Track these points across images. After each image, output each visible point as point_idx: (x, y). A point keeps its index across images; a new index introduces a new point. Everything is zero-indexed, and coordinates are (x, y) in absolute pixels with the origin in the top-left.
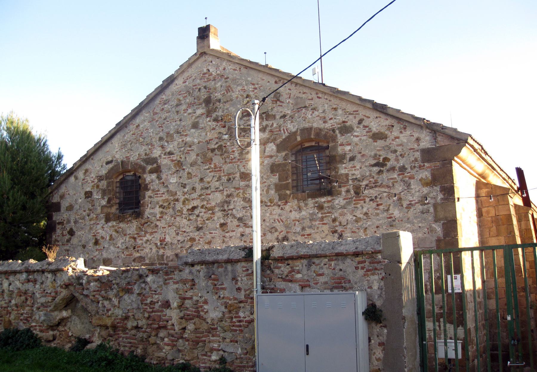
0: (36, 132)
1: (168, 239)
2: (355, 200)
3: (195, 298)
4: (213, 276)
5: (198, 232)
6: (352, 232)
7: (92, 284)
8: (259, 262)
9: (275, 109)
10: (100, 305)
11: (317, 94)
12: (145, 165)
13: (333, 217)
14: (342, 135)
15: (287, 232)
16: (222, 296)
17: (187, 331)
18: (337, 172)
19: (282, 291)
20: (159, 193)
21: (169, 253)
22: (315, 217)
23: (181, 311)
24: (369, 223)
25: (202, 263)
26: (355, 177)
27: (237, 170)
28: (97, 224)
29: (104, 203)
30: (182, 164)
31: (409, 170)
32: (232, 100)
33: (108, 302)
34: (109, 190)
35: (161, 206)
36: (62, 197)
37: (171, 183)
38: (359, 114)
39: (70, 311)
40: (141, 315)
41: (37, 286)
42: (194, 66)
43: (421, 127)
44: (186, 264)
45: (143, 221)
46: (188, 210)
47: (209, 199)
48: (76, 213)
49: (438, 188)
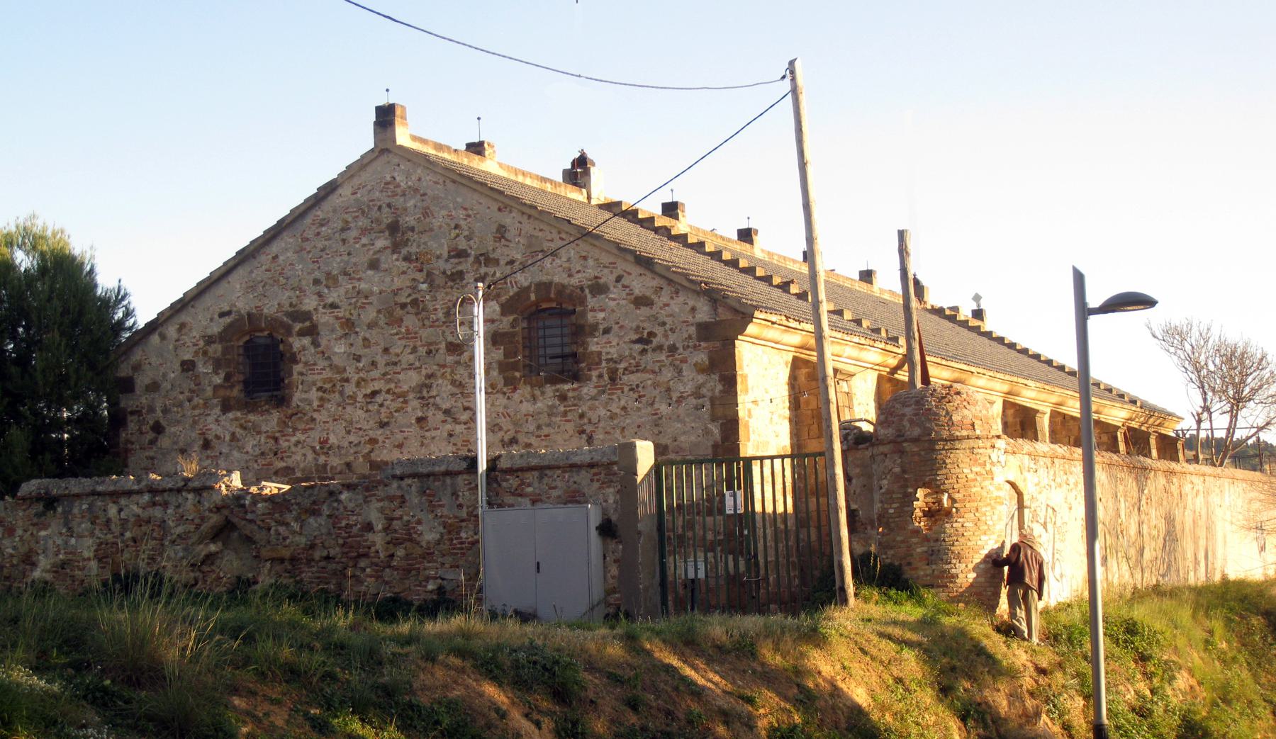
0: (77, 246)
1: (333, 440)
2: (609, 389)
3: (405, 518)
4: (428, 491)
5: (382, 430)
6: (606, 433)
7: (260, 505)
8: (485, 474)
9: (499, 251)
10: (272, 531)
11: (559, 233)
12: (290, 322)
13: (580, 411)
14: (594, 296)
15: (516, 432)
16: (439, 514)
17: (395, 558)
18: (586, 349)
19: (511, 506)
20: (316, 367)
21: (335, 461)
22: (555, 410)
23: (387, 535)
24: (628, 421)
25: (414, 475)
26: (610, 357)
27: (441, 338)
28: (206, 415)
29: (218, 380)
30: (353, 324)
31: (681, 350)
32: (431, 230)
33: (284, 528)
34: (226, 359)
35: (320, 389)
36: (137, 368)
37: (336, 353)
38: (616, 268)
39: (220, 544)
40: (333, 542)
41: (169, 511)
42: (369, 169)
43: (698, 293)
44: (394, 477)
45: (290, 412)
46: (365, 396)
47: (399, 381)
48: (166, 396)
49: (716, 377)
